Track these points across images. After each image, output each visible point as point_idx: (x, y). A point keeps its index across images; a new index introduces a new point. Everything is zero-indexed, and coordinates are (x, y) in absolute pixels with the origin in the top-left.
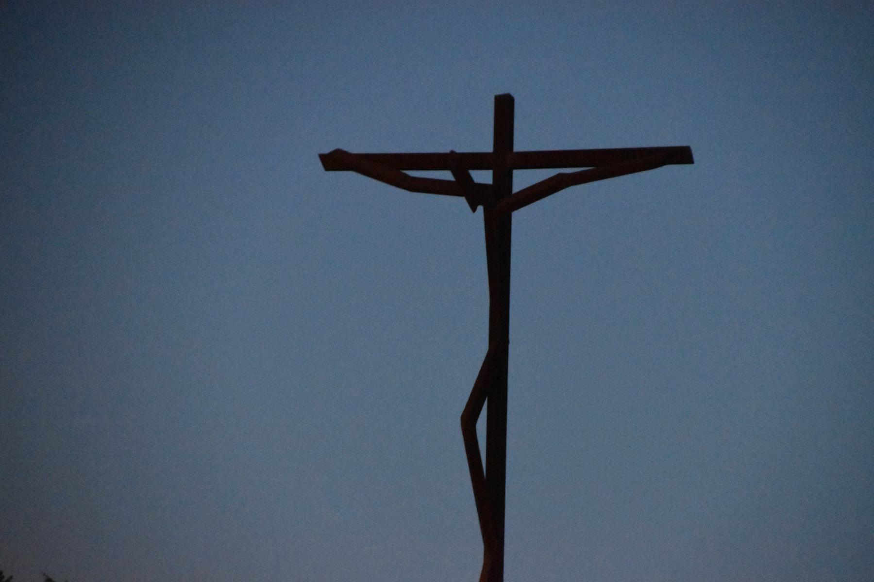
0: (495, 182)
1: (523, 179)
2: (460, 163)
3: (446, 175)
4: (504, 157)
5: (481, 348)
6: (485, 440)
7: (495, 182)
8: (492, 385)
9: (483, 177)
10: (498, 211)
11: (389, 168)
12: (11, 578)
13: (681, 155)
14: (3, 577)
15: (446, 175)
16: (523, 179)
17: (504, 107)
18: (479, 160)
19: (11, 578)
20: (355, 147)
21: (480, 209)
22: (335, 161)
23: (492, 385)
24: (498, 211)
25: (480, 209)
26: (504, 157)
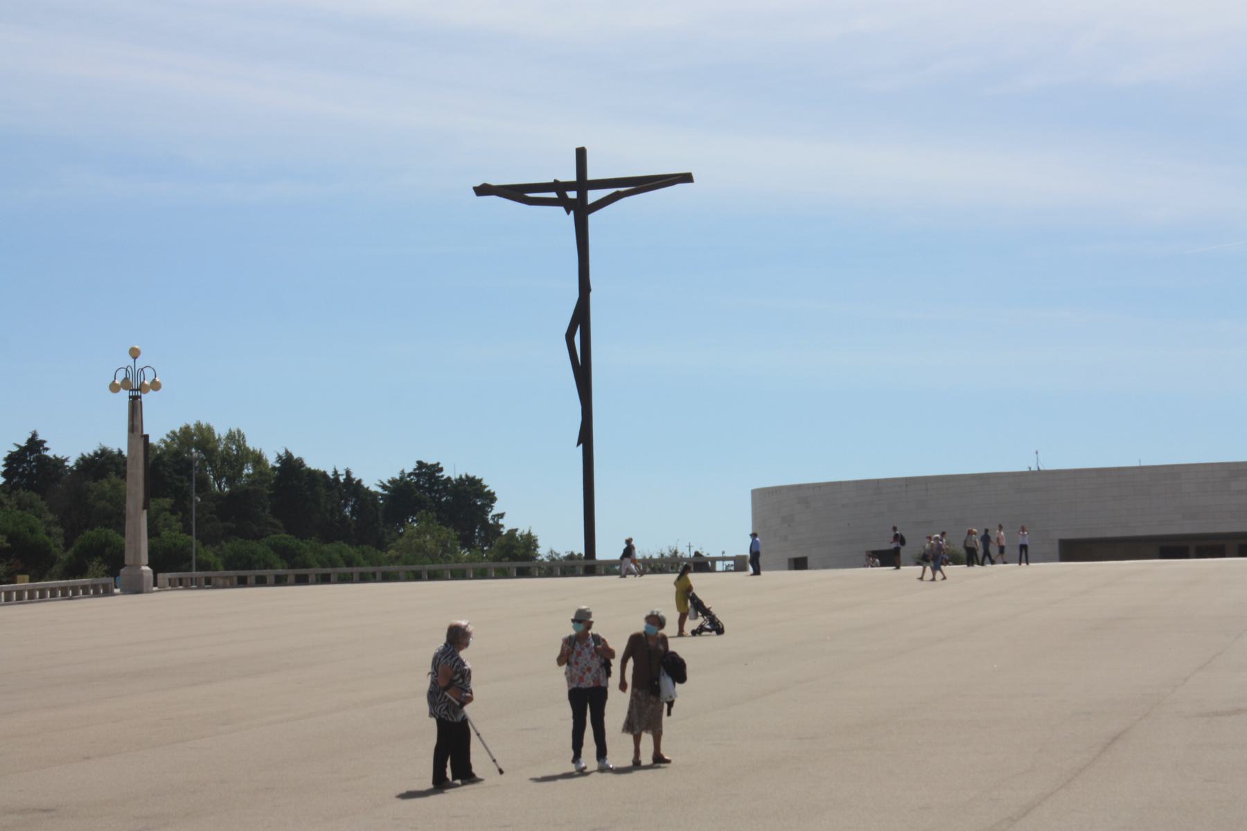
0: (577, 196)
1: (593, 196)
2: (557, 186)
3: (553, 195)
4: (583, 184)
6: (585, 741)
8: (581, 317)
9: (572, 195)
10: (581, 212)
11: (516, 193)
13: (687, 178)
15: (553, 195)
16: (593, 196)
17: (581, 154)
18: (569, 186)
22: (483, 190)
23: (581, 317)
24: (581, 212)
26: (583, 184)
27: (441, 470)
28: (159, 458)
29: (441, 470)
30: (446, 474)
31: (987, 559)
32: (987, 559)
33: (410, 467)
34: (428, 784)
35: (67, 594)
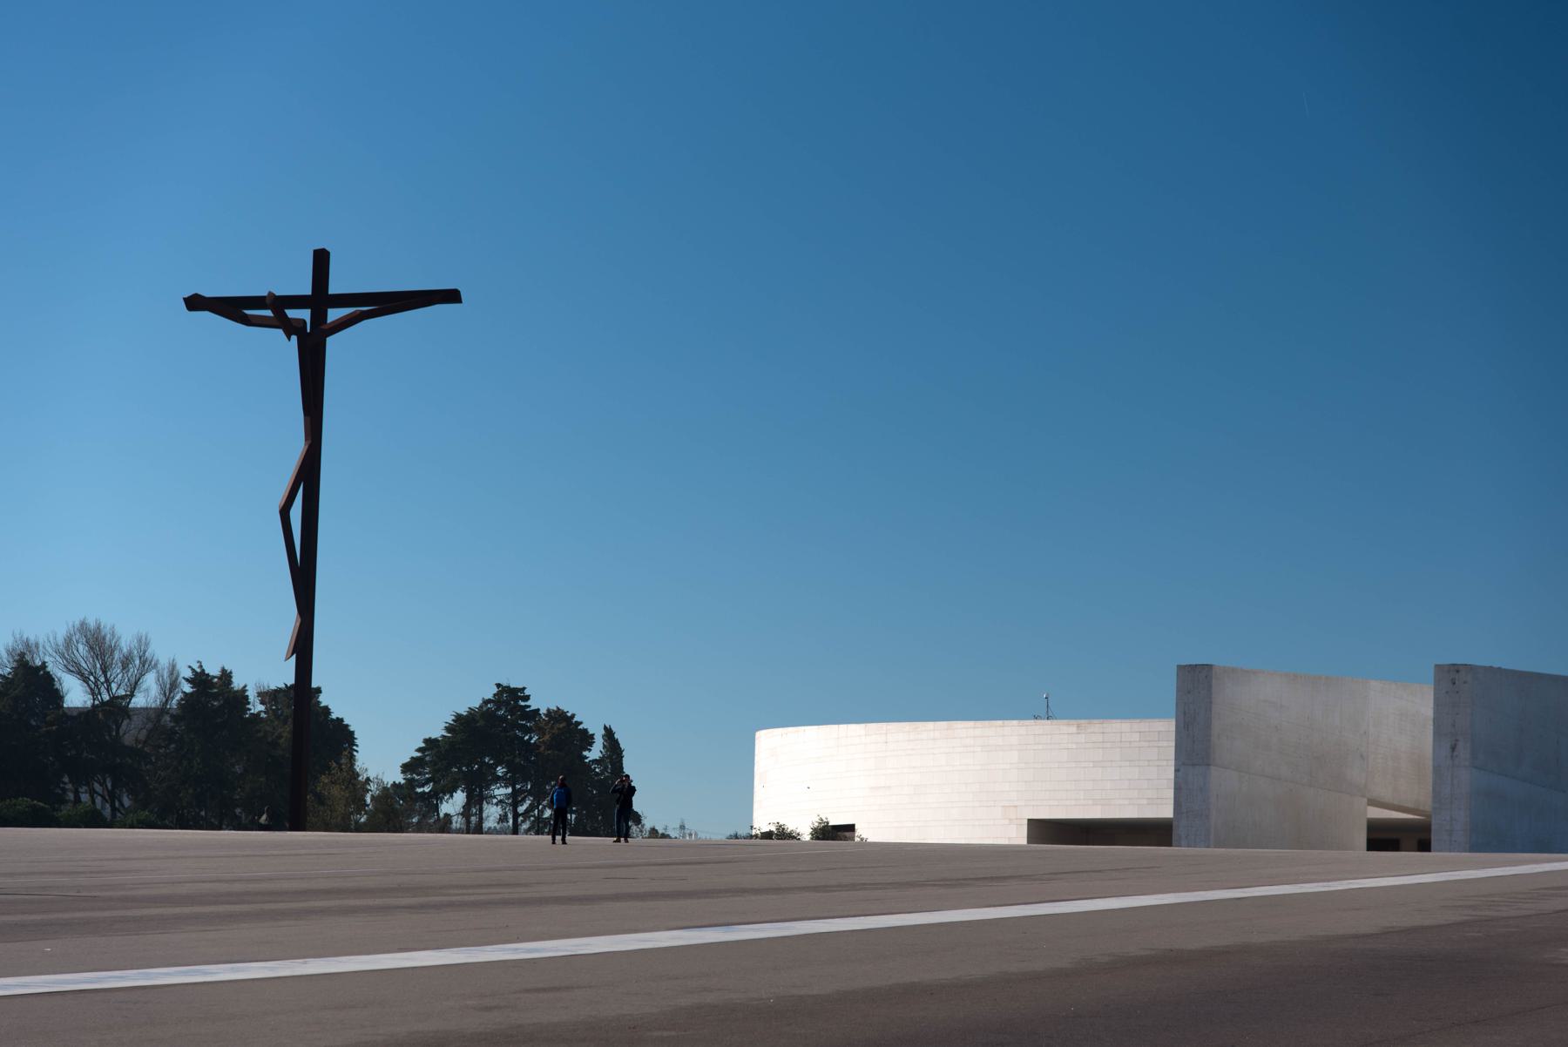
0: (311, 319)
1: (334, 314)
2: (279, 304)
3: (268, 313)
4: (320, 298)
5: (297, 447)
7: (311, 319)
8: (308, 475)
9: (305, 314)
11: (232, 308)
13: (452, 296)
14: (241, 698)
15: (268, 313)
16: (334, 314)
17: (321, 260)
20: (208, 293)
21: (294, 338)
22: (195, 303)
23: (308, 475)
25: (294, 338)
27: (527, 698)
29: (527, 698)
30: (533, 704)
33: (490, 692)
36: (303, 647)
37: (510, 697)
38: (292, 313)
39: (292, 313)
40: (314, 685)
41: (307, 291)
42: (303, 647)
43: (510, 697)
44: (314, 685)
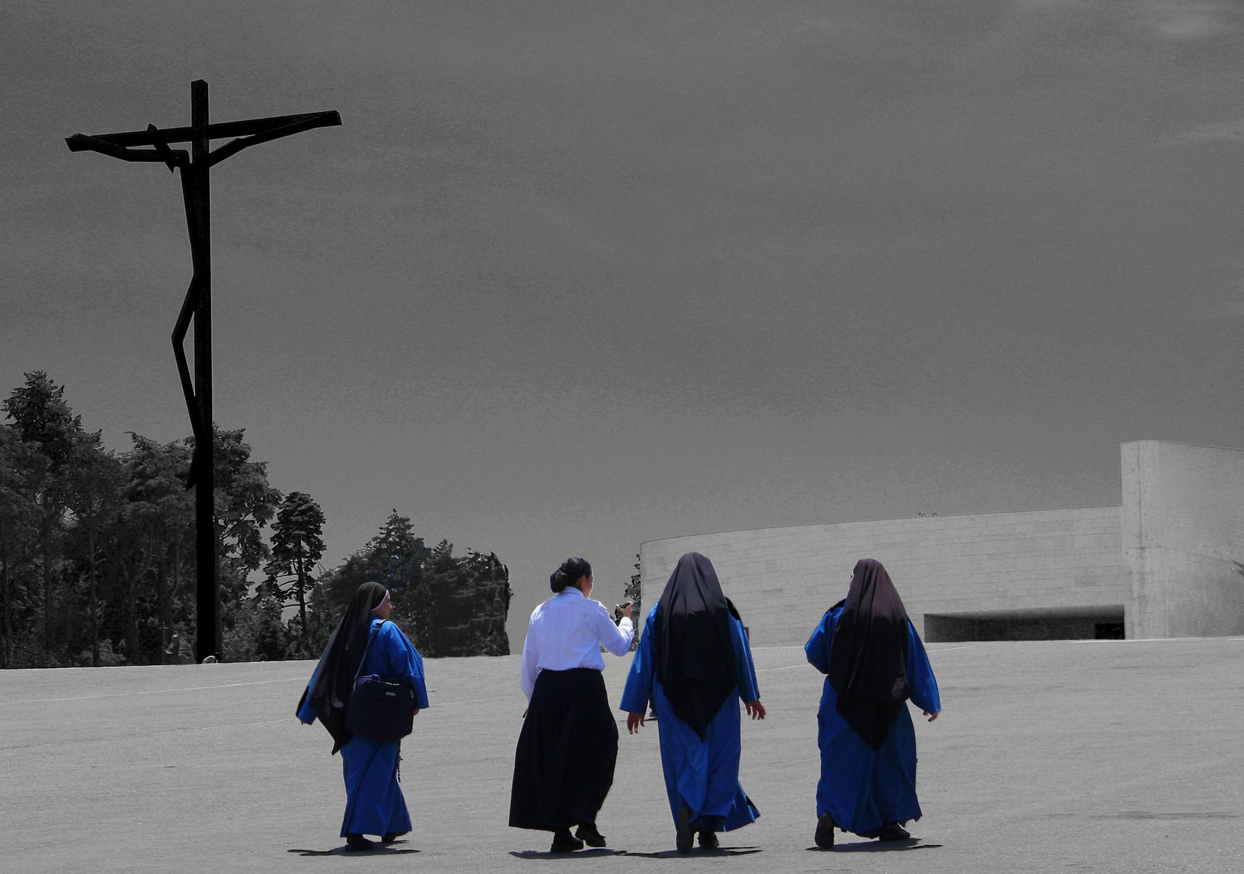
0: (193, 150)
1: (215, 145)
3: (152, 147)
4: (201, 129)
5: (188, 272)
8: (655, 855)
9: (187, 146)
11: (115, 146)
12: (334, 753)
13: (331, 119)
15: (152, 147)
16: (215, 145)
17: (200, 91)
18: (179, 134)
19: (334, 753)
21: (177, 169)
22: (78, 143)
23: (655, 855)
25: (177, 169)
26: (201, 129)
28: (259, 487)
31: (299, 619)
32: (299, 619)
34: (673, 847)
35: (1105, 608)
36: (199, 404)
37: (425, 705)
38: (173, 146)
39: (173, 146)
40: (317, 721)
41: (188, 123)
42: (199, 404)
43: (425, 705)
44: (317, 721)
